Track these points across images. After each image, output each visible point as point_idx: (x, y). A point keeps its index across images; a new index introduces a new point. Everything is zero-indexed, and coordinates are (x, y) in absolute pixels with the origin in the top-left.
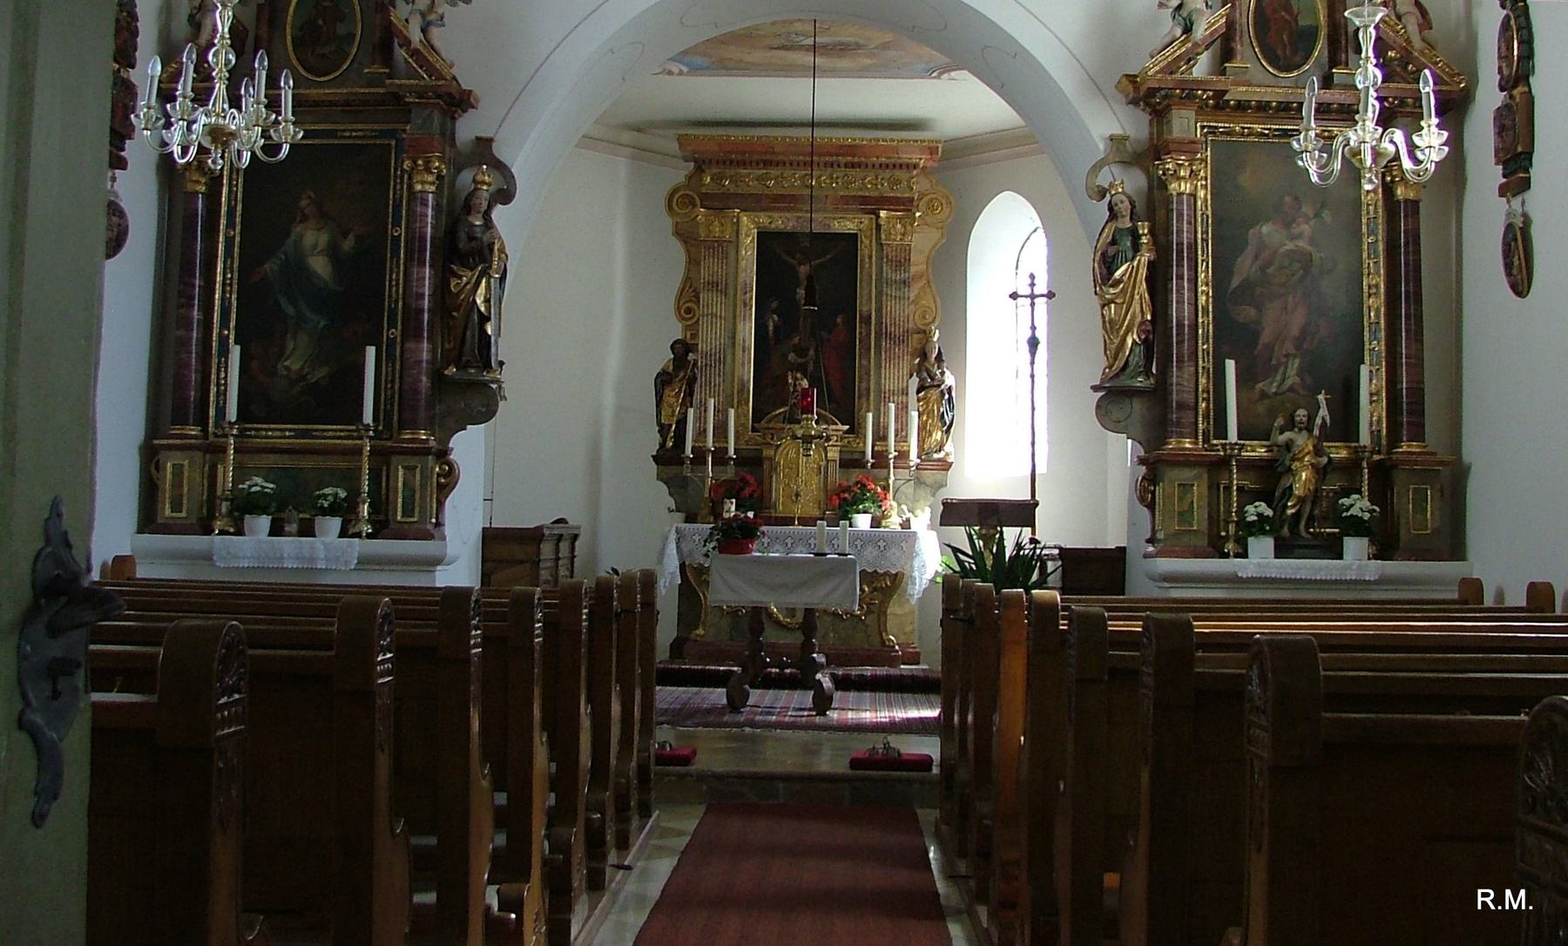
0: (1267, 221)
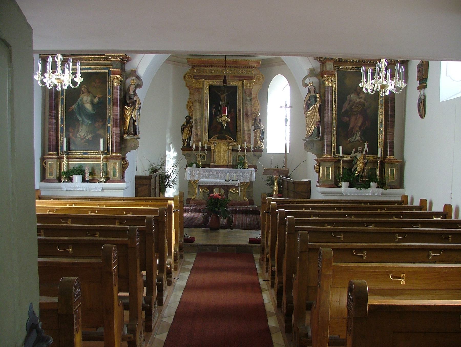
0: (352, 93)
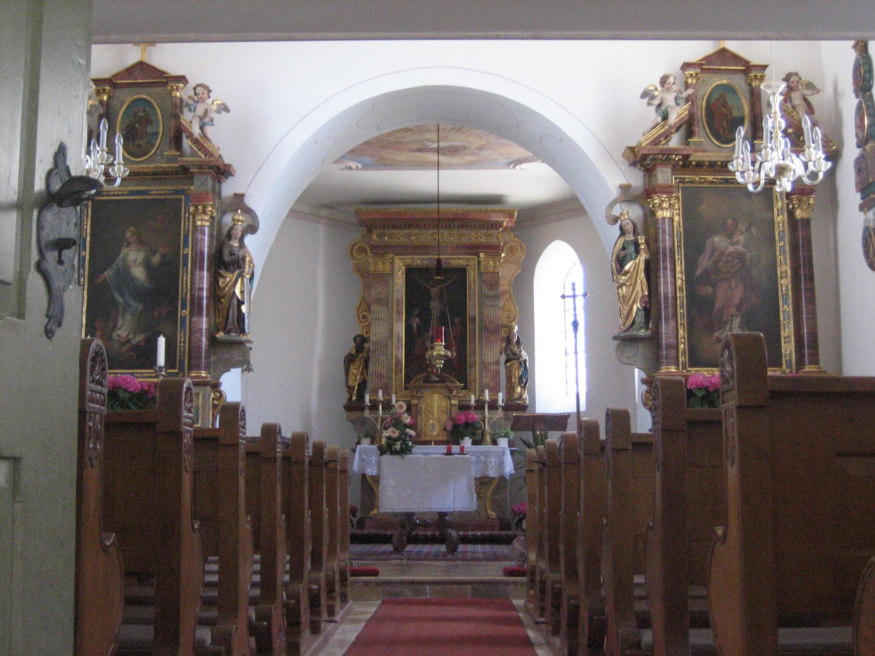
0: (716, 233)
